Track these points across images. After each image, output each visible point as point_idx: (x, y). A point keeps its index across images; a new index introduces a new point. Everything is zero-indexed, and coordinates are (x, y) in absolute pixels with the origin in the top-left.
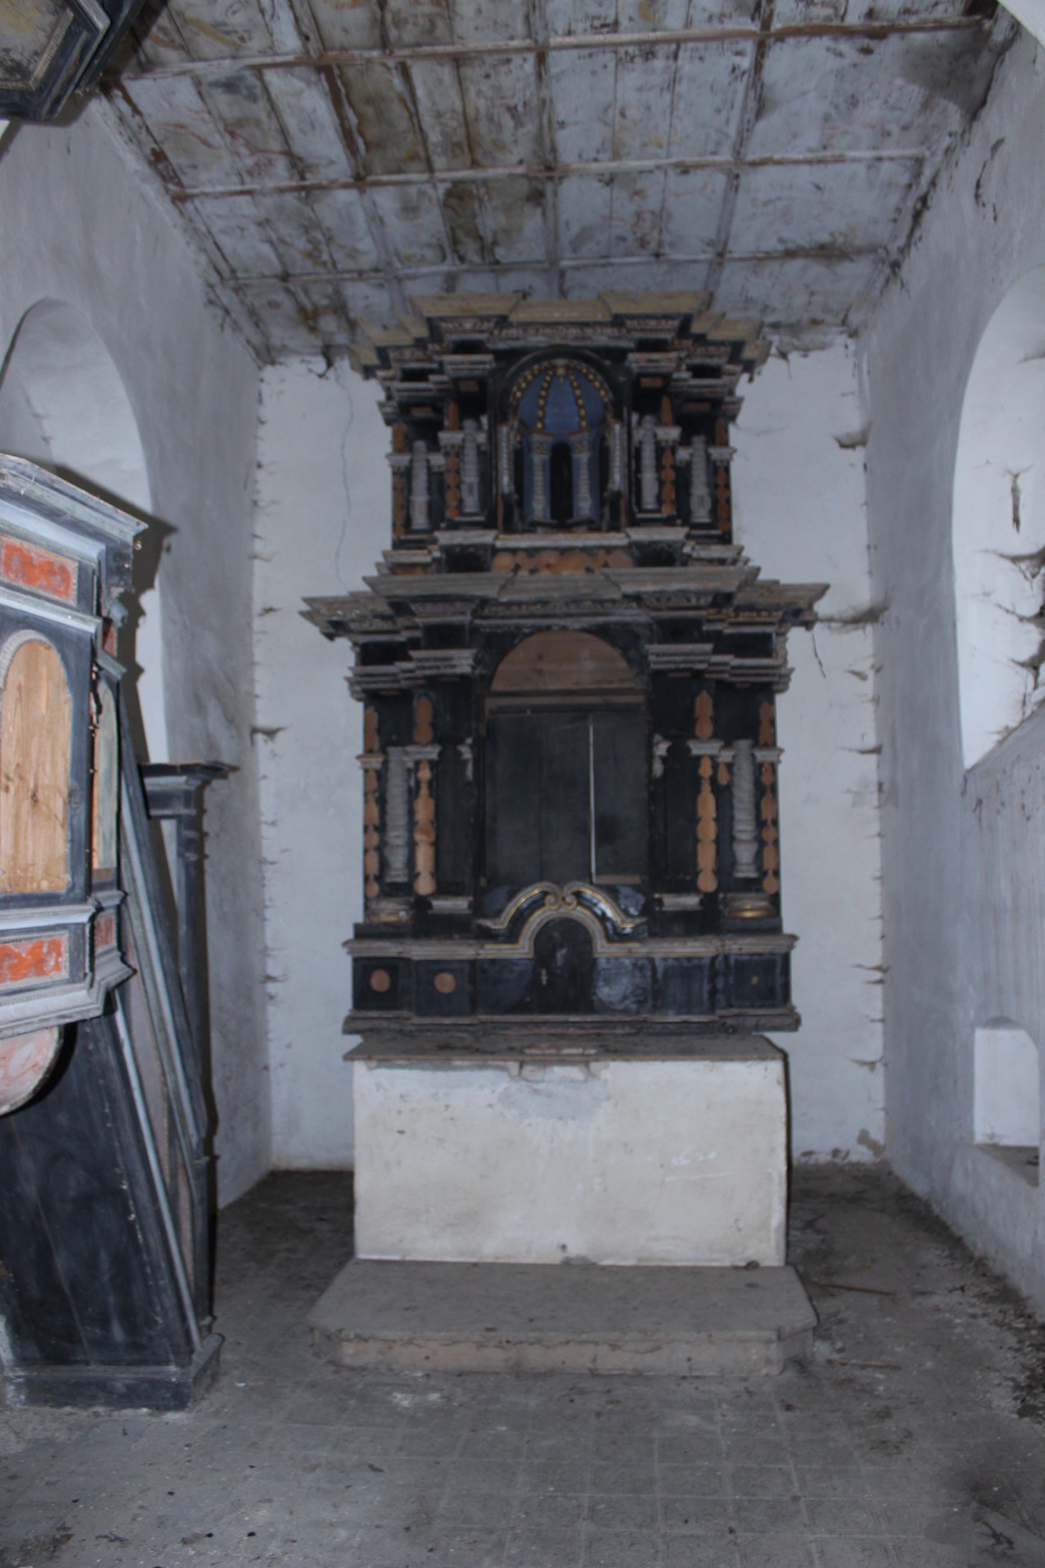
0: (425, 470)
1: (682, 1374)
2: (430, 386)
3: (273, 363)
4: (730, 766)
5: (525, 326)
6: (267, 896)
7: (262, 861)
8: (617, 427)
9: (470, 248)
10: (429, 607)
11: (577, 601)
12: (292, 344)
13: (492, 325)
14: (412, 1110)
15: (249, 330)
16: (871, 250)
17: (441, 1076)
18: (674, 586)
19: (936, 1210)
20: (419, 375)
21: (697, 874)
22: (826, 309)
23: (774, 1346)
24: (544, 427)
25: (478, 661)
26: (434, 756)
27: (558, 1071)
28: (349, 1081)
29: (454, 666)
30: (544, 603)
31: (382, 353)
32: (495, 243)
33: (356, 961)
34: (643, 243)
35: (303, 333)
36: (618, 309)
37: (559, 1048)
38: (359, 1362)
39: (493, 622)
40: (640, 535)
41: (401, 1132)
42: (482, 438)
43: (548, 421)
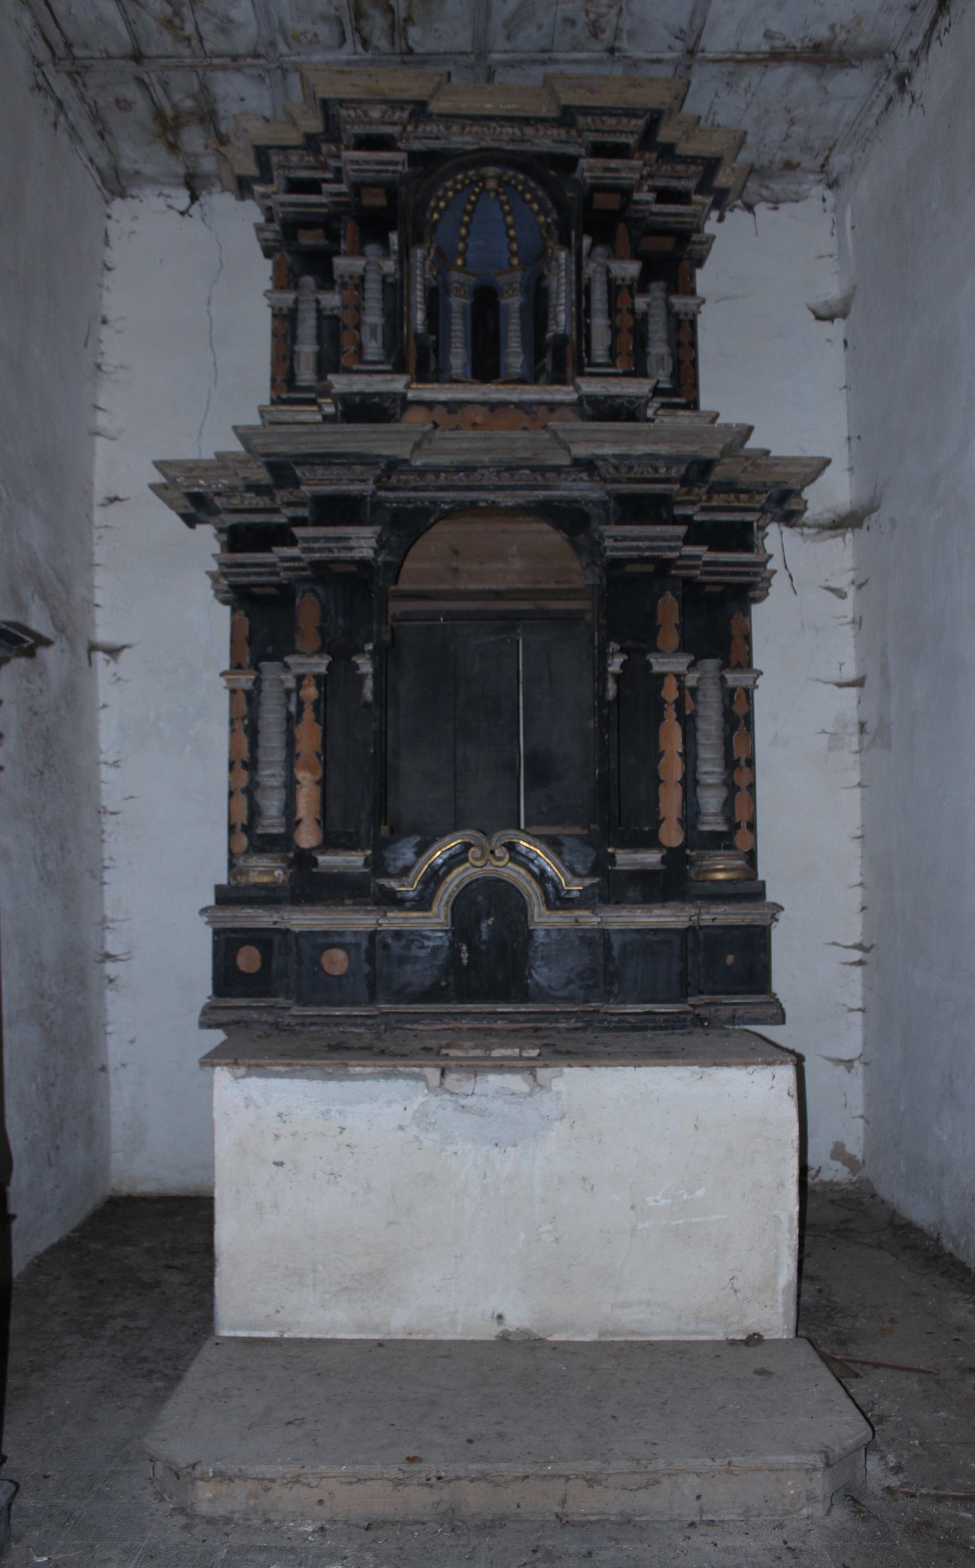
0: (313, 314)
1: (689, 1519)
2: (324, 200)
3: (123, 195)
4: (694, 691)
5: (449, 118)
6: (106, 855)
7: (101, 811)
8: (563, 255)
9: (377, 25)
10: (319, 472)
11: (511, 469)
12: (148, 169)
13: (405, 115)
14: (294, 1134)
15: (92, 142)
16: (877, 53)
17: (333, 1087)
18: (641, 449)
19: (949, 1246)
20: (312, 186)
21: (659, 823)
22: (806, 147)
23: (819, 1475)
24: (465, 263)
25: (382, 545)
26: (322, 670)
27: (494, 1080)
28: (211, 1086)
29: (351, 549)
30: (469, 469)
31: (262, 154)
32: (408, 20)
33: (216, 932)
34: (595, 30)
35: (161, 152)
36: (570, 98)
37: (489, 1048)
38: (221, 1510)
39: (402, 494)
40: (591, 387)
41: (280, 1164)
42: (389, 266)
43: (469, 256)
